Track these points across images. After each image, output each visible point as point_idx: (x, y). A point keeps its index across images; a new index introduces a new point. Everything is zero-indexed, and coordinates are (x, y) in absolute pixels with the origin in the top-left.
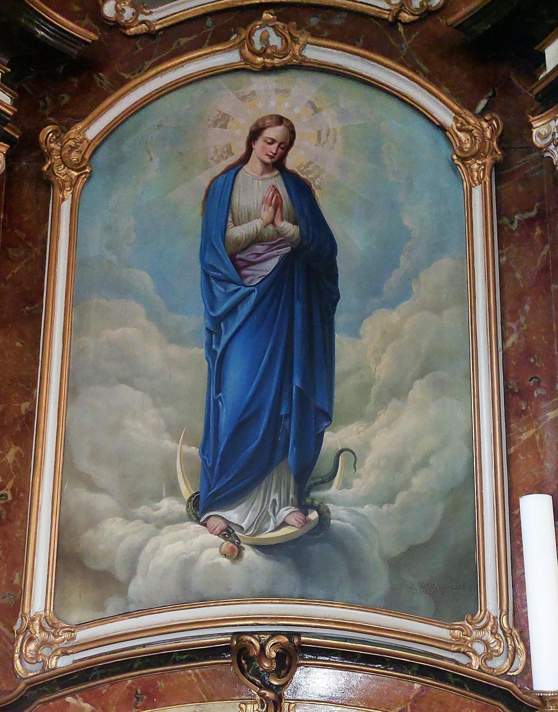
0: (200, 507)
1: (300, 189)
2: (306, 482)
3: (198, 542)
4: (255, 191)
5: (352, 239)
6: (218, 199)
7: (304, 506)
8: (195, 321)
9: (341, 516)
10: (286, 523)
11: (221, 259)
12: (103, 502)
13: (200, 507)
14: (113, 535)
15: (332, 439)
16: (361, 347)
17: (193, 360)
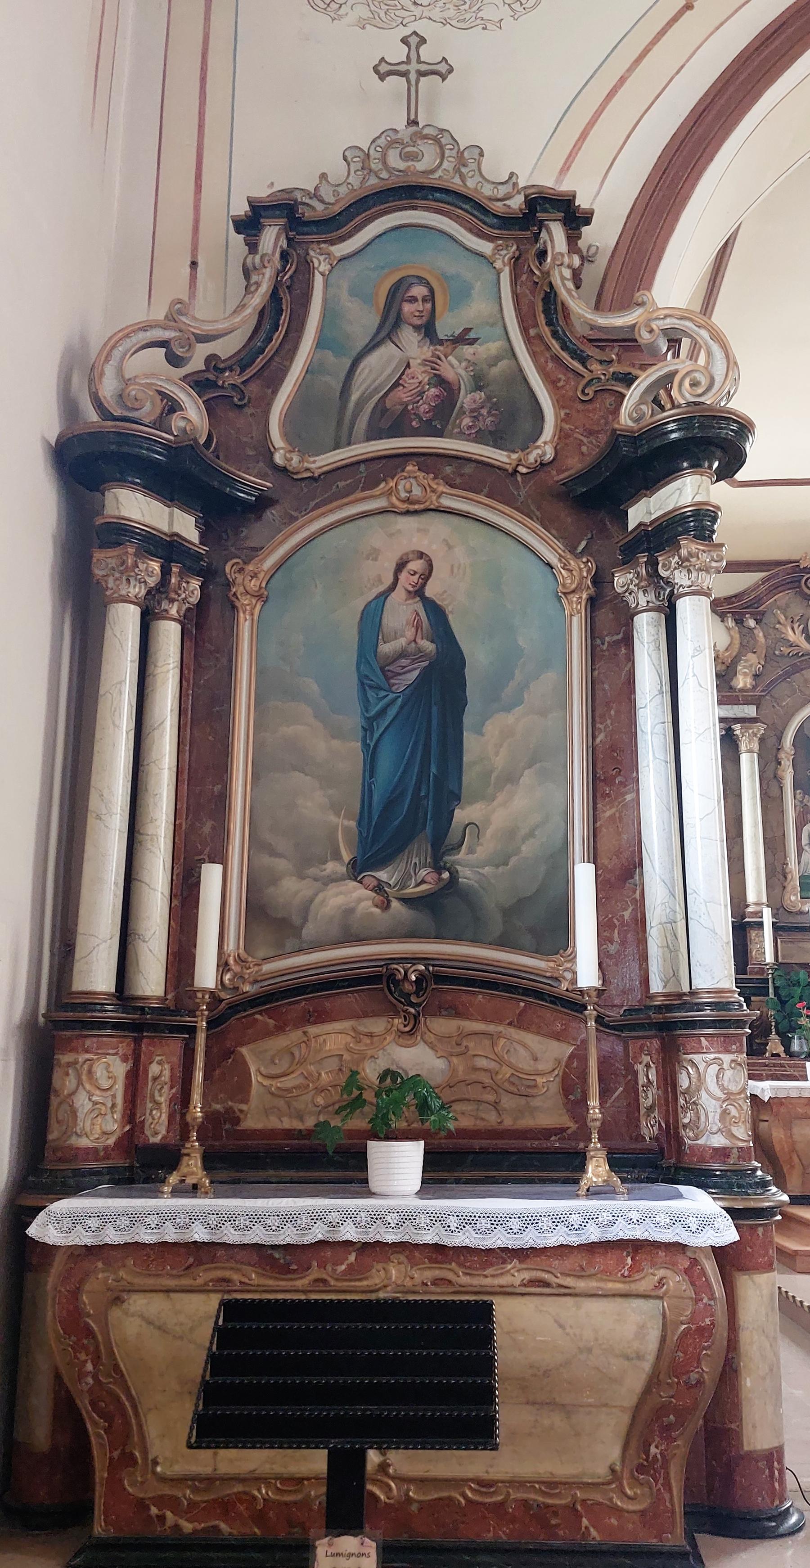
0: (357, 869)
1: (436, 613)
2: (441, 848)
3: (353, 897)
4: (401, 614)
5: (478, 656)
6: (371, 619)
7: (438, 869)
8: (353, 720)
9: (467, 876)
10: (424, 880)
11: (374, 671)
12: (281, 865)
13: (357, 869)
14: (290, 889)
15: (461, 815)
16: (486, 742)
17: (347, 756)
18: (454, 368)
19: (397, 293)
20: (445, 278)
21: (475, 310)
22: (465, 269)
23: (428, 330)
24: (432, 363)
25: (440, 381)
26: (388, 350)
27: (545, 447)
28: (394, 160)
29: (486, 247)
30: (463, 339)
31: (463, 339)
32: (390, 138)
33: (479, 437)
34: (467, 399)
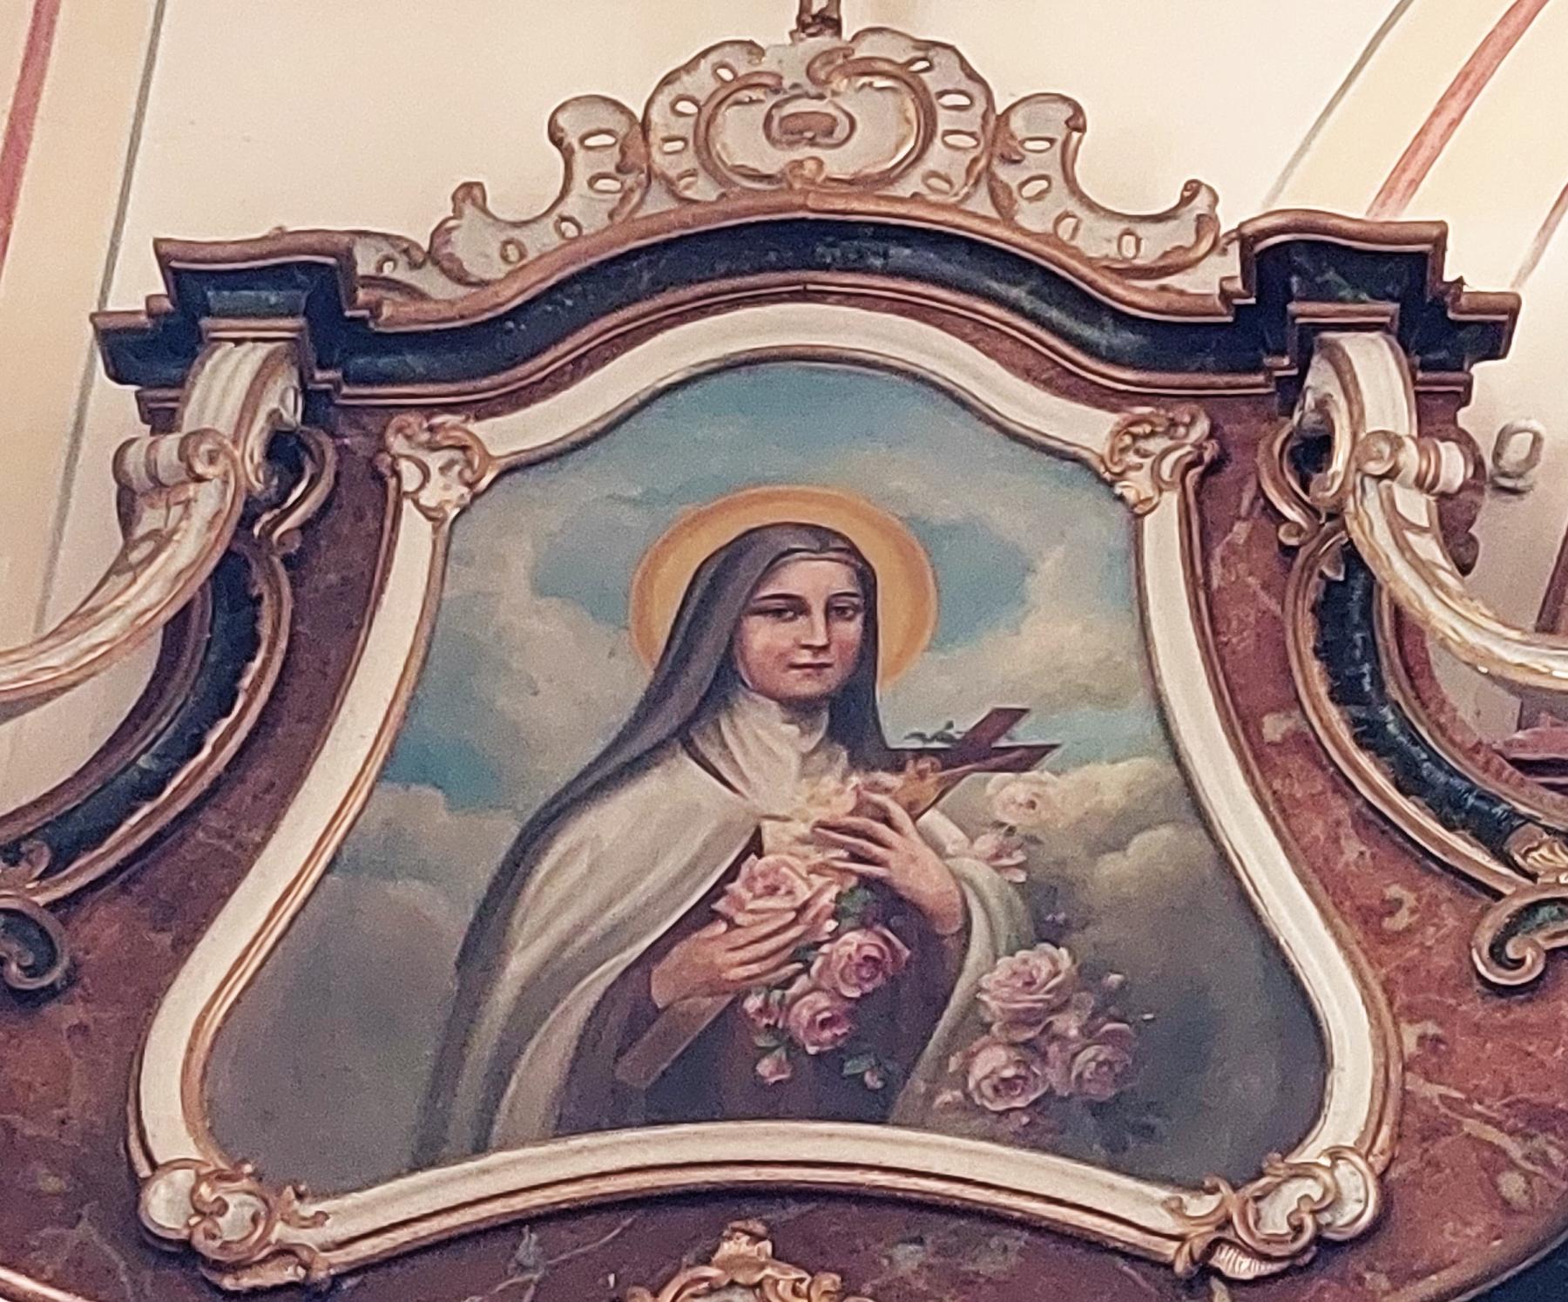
18: (947, 853)
19: (729, 583)
20: (923, 538)
21: (1043, 644)
22: (1006, 504)
23: (845, 717)
24: (855, 838)
25: (886, 904)
26: (676, 784)
27: (1336, 1169)
28: (743, 140)
29: (1089, 428)
30: (989, 746)
31: (989, 746)
32: (740, 78)
33: (1045, 1127)
34: (993, 974)
